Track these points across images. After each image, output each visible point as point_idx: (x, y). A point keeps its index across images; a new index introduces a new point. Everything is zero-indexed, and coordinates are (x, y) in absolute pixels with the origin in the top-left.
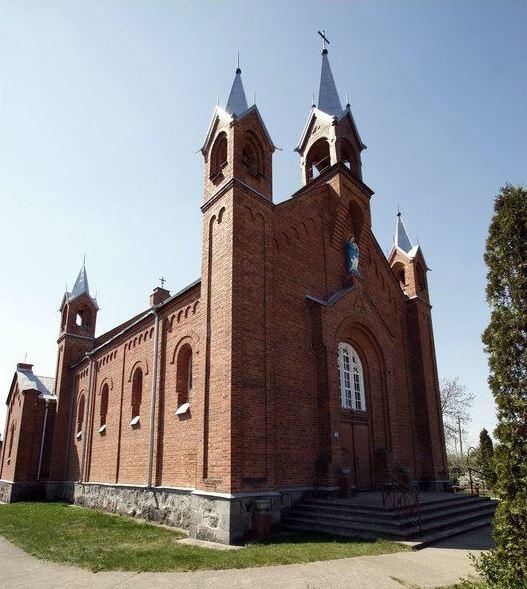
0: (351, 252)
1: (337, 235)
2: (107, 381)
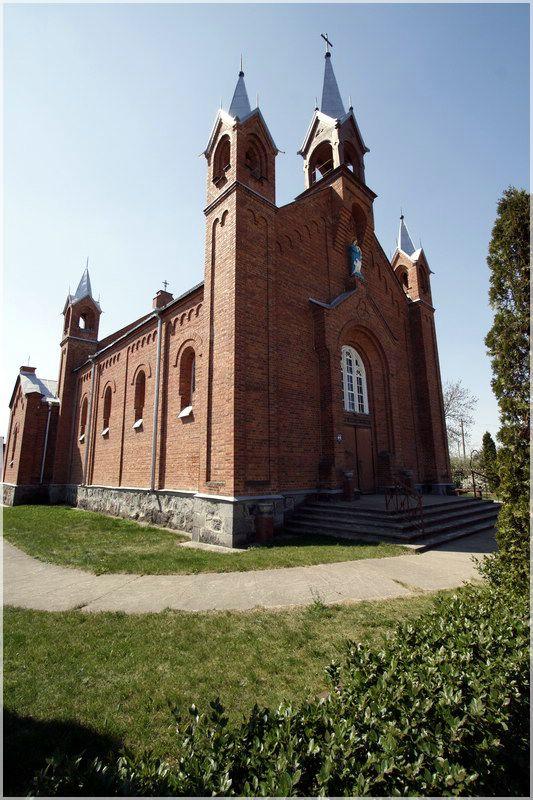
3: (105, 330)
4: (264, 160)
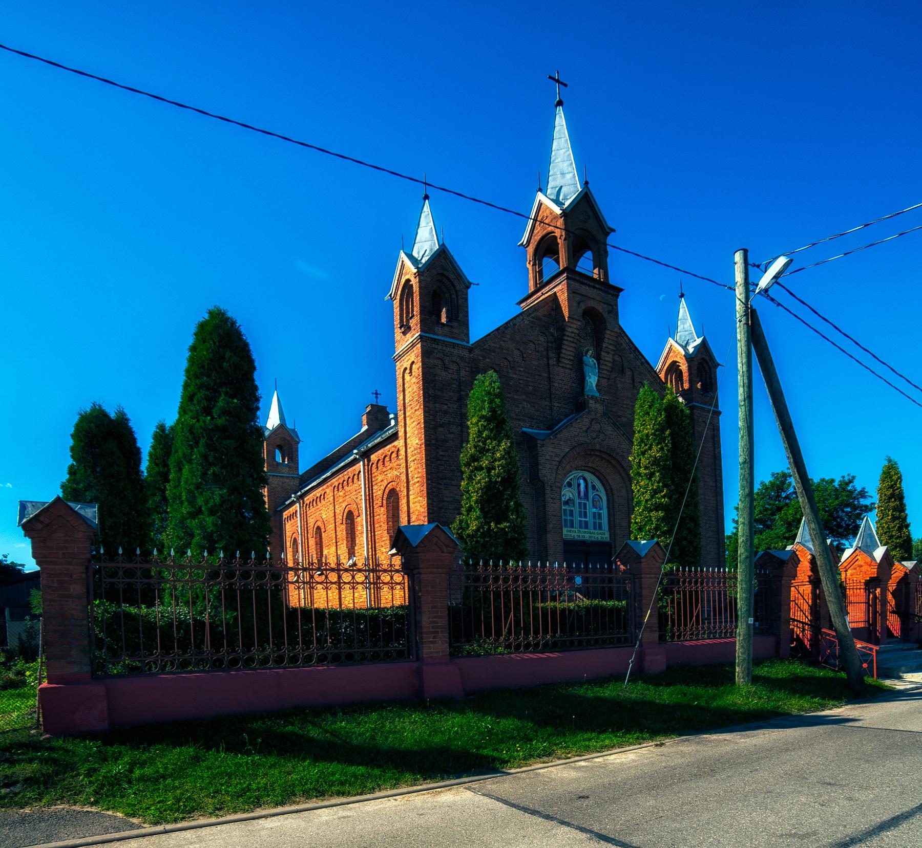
0: (586, 369)
1: (568, 351)
2: (319, 523)
3: (305, 463)
4: (454, 296)
